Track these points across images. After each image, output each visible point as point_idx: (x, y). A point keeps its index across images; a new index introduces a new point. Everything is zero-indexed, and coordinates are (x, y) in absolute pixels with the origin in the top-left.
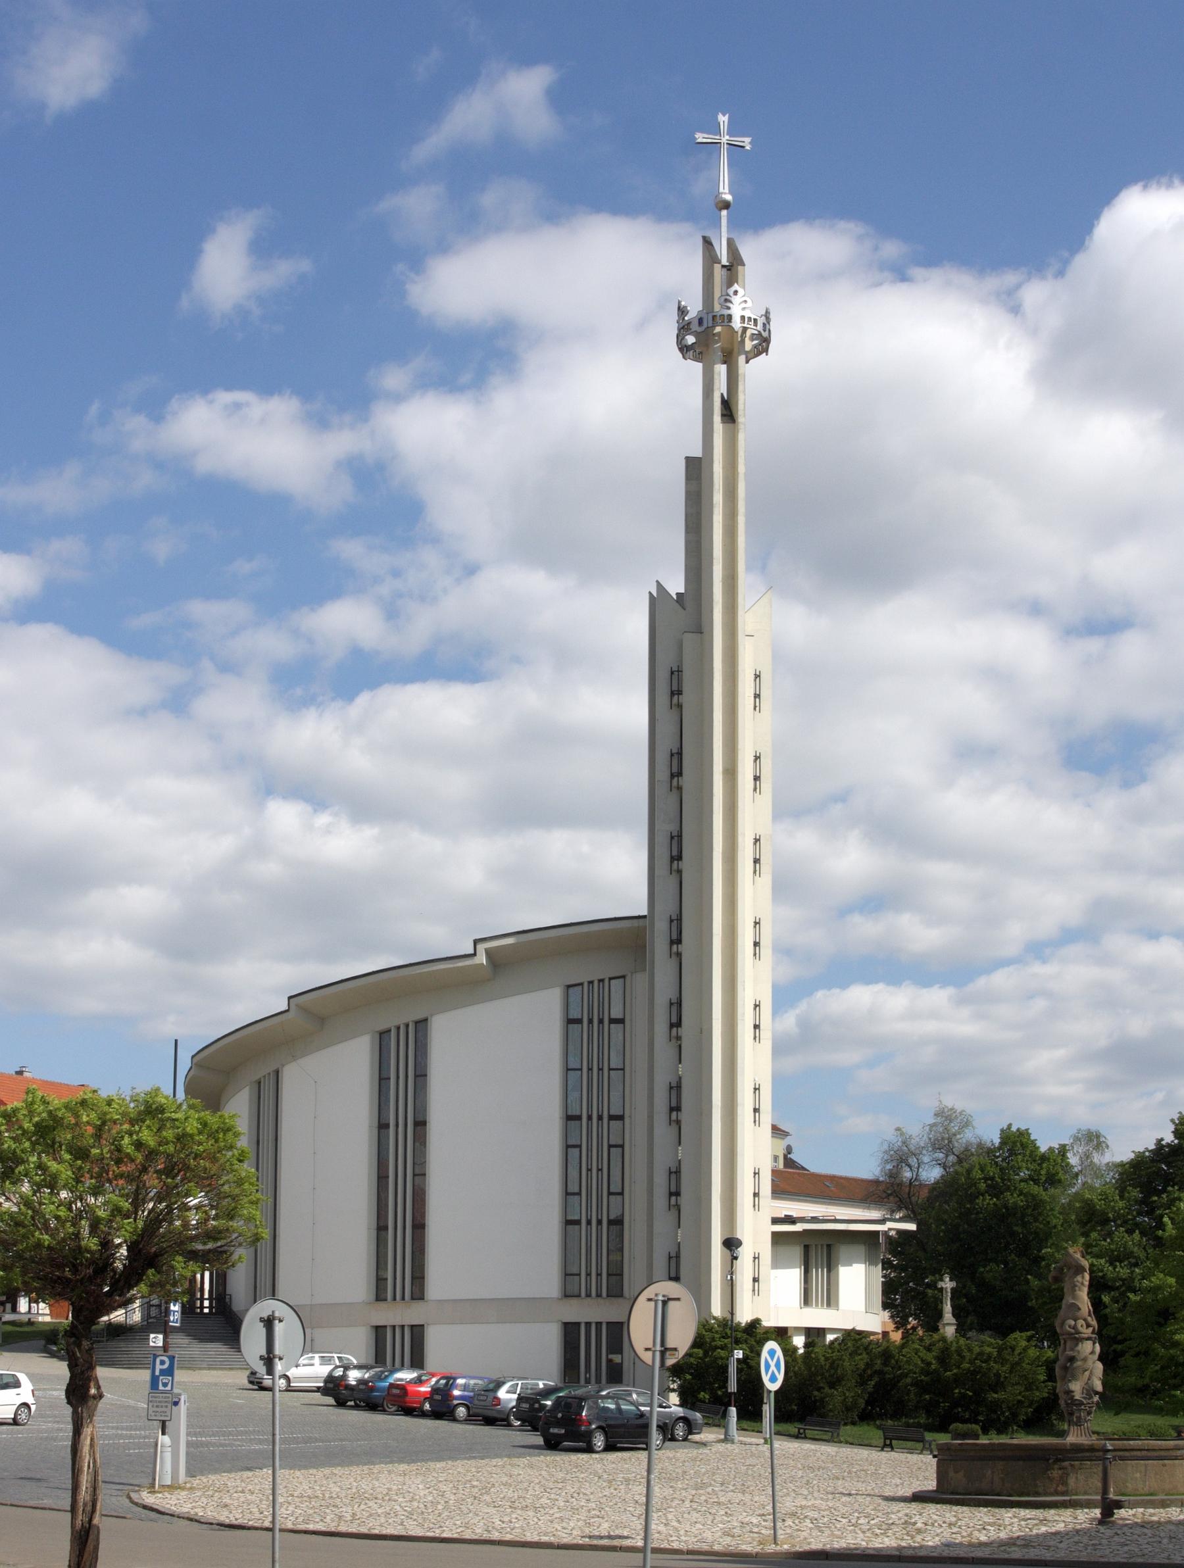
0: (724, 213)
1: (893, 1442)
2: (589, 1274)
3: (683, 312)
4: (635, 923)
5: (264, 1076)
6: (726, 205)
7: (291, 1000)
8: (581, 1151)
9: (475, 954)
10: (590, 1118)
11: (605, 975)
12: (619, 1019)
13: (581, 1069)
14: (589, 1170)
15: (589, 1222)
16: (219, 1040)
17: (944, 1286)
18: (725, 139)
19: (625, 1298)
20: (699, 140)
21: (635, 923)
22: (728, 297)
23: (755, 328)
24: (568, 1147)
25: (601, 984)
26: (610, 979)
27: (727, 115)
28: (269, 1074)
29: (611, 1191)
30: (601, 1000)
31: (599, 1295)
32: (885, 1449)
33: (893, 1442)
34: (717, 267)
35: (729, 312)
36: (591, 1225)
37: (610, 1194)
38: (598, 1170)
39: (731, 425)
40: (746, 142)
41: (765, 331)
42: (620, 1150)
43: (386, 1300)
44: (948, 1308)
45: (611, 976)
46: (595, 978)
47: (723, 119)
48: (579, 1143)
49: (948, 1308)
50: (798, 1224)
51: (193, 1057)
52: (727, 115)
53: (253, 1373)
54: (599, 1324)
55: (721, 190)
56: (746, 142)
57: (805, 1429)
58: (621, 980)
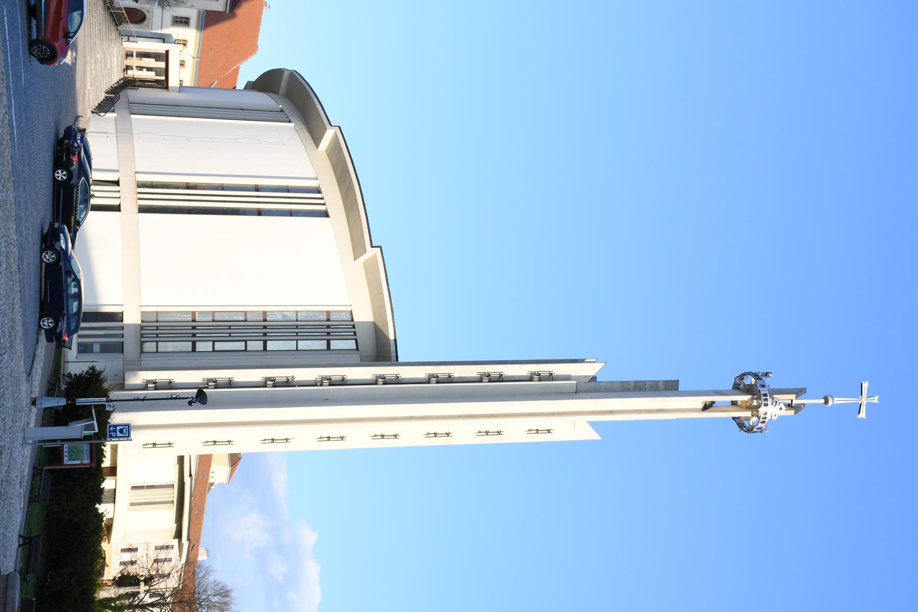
0: (823, 401)
3: (766, 375)
4: (393, 355)
5: (286, 115)
6: (826, 402)
7: (338, 128)
9: (372, 247)
11: (358, 337)
16: (309, 85)
17: (141, 586)
18: (864, 400)
19: (141, 355)
20: (864, 385)
21: (393, 355)
22: (778, 404)
23: (760, 422)
25: (353, 334)
26: (356, 340)
27: (878, 402)
28: (288, 117)
32: (21, 539)
34: (793, 397)
39: (701, 409)
40: (863, 415)
41: (757, 429)
43: (123, 343)
46: (357, 330)
47: (875, 400)
51: (296, 71)
52: (878, 402)
54: (123, 336)
55: (835, 399)
57: (41, 474)
58: (355, 347)
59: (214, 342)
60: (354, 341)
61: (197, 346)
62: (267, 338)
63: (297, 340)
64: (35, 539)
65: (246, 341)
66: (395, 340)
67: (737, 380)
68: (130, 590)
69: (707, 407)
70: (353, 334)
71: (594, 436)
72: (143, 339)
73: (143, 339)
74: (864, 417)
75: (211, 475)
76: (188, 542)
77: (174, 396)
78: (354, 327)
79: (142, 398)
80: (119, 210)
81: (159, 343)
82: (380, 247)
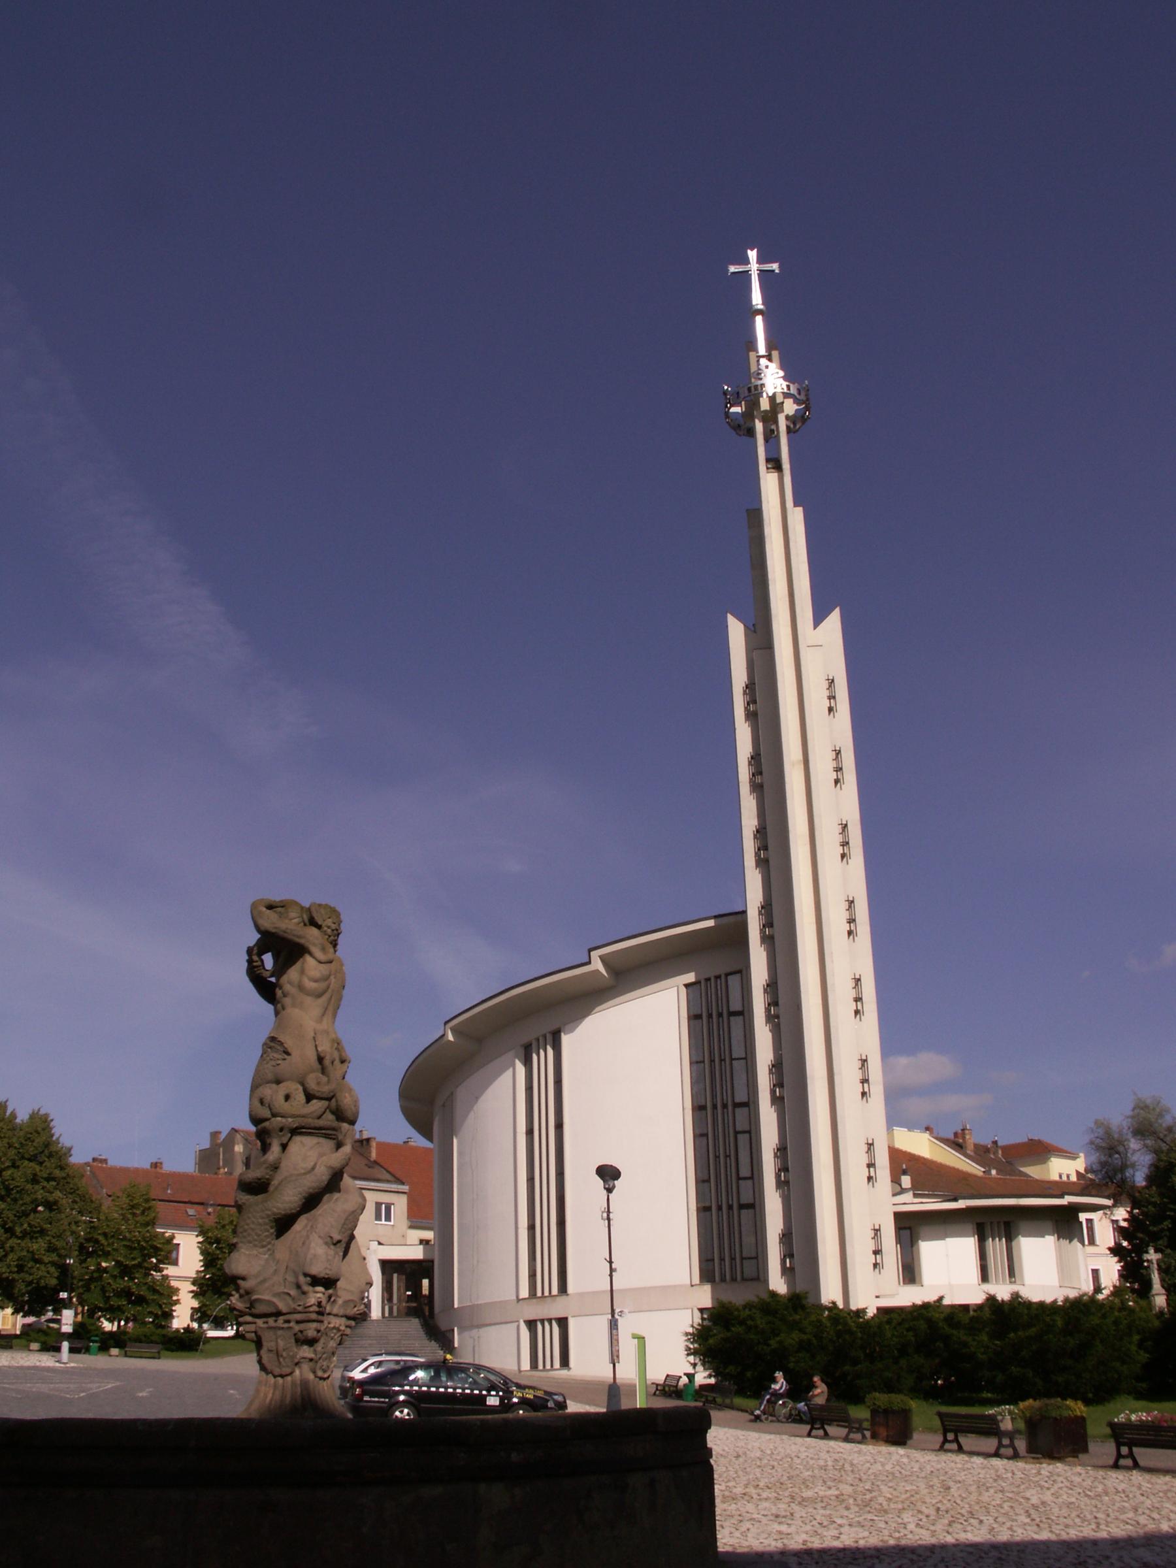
1: (1135, 1449)
2: (722, 1259)
4: (731, 919)
8: (708, 1139)
9: (589, 963)
10: (715, 1107)
11: (721, 971)
12: (739, 1107)
13: (703, 1062)
14: (717, 1157)
15: (720, 1208)
24: (752, 1178)
26: (727, 975)
29: (745, 1255)
30: (729, 1181)
31: (734, 1279)
33: (1135, 1449)
35: (761, 382)
36: (716, 1108)
37: (739, 1178)
38: (721, 1060)
40: (775, 267)
42: (747, 1135)
44: (1156, 1278)
45: (728, 970)
47: (752, 254)
48: (706, 1132)
49: (1156, 1278)
50: (960, 1201)
53: (250, 1155)
56: (775, 267)
58: (738, 975)
59: (739, 1178)
60: (730, 978)
61: (746, 1202)
62: (730, 1103)
63: (732, 1059)
64: (946, 1423)
65: (736, 1133)
66: (715, 917)
67: (741, 433)
68: (1156, 1273)
69: (775, 463)
70: (709, 982)
71: (834, 620)
72: (739, 1278)
73: (739, 1278)
74: (749, 252)
75: (1064, 1178)
76: (1066, 1197)
77: (605, 1215)
78: (708, 980)
79: (608, 1264)
80: (566, 1319)
81: (744, 1256)
82: (590, 951)
